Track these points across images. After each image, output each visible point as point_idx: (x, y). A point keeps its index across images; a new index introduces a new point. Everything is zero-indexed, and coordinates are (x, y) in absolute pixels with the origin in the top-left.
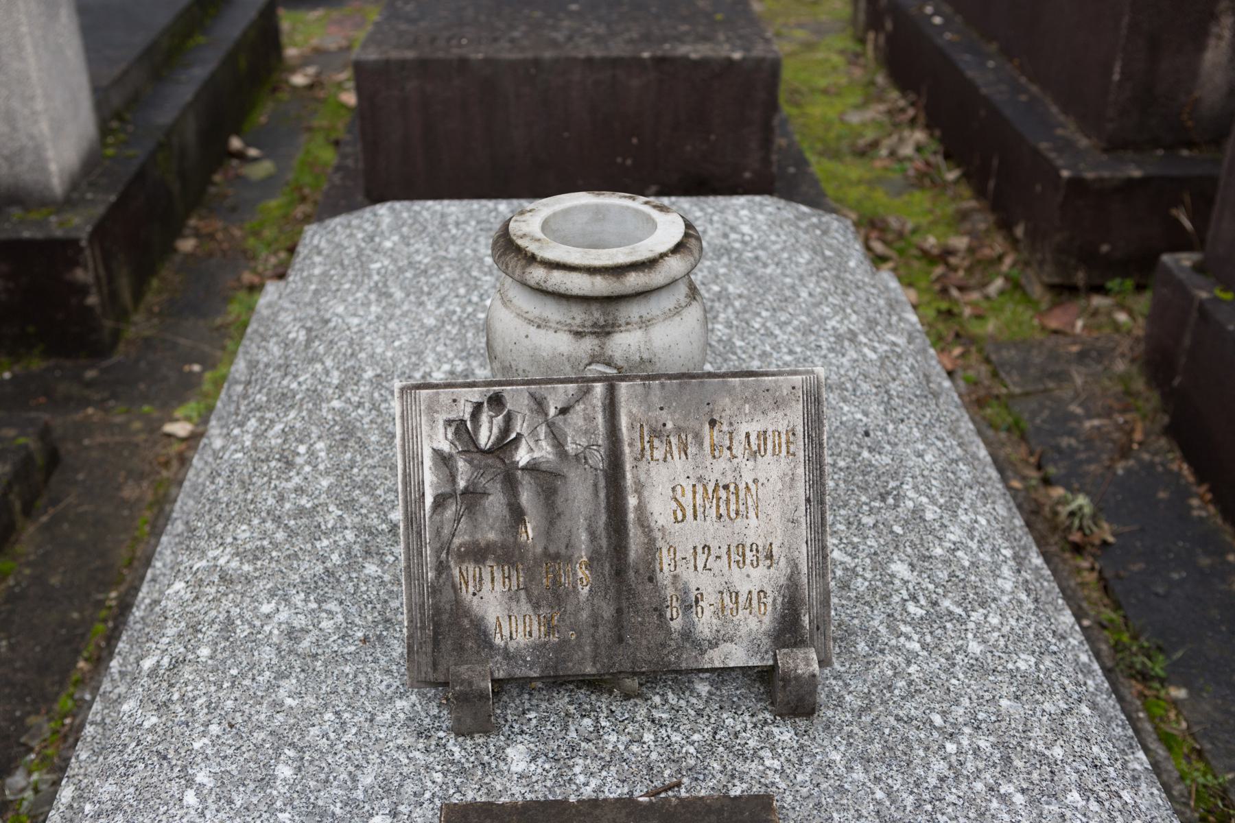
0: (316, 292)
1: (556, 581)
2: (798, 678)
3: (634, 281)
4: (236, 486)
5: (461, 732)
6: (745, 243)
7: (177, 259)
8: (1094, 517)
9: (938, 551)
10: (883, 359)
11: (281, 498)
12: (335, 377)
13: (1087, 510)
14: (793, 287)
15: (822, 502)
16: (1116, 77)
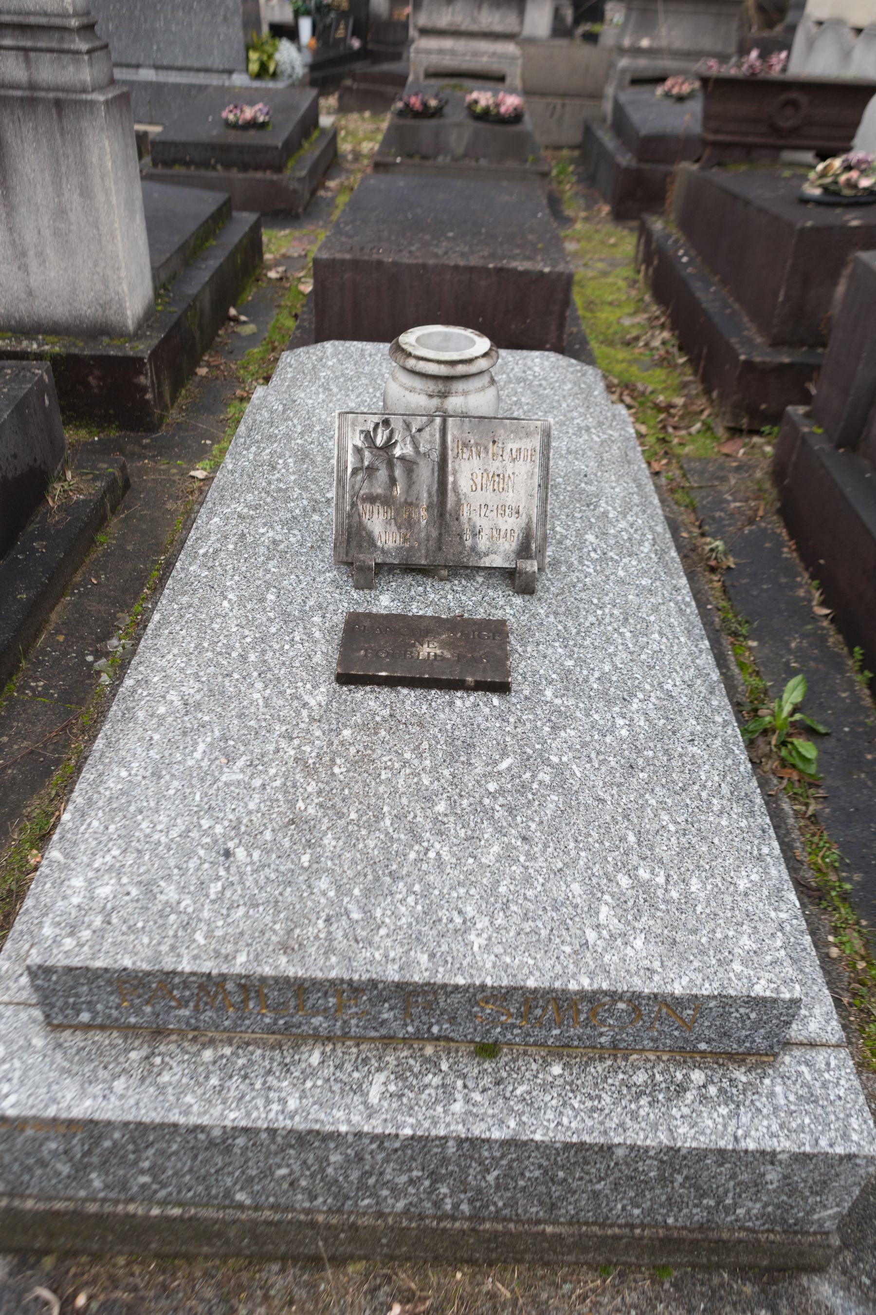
0: (288, 386)
1: (410, 517)
2: (526, 573)
3: (461, 369)
4: (245, 477)
5: (357, 587)
6: (535, 377)
7: (197, 379)
8: (725, 554)
9: (612, 531)
10: (603, 442)
11: (269, 483)
12: (299, 429)
13: (721, 548)
14: (558, 401)
15: (547, 488)
16: (781, 298)
